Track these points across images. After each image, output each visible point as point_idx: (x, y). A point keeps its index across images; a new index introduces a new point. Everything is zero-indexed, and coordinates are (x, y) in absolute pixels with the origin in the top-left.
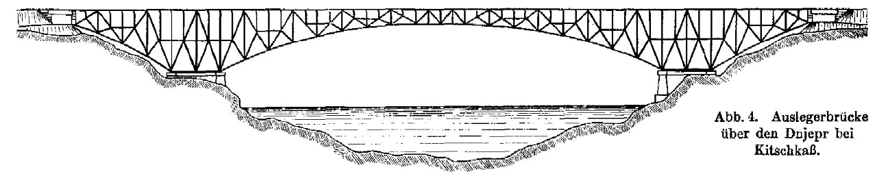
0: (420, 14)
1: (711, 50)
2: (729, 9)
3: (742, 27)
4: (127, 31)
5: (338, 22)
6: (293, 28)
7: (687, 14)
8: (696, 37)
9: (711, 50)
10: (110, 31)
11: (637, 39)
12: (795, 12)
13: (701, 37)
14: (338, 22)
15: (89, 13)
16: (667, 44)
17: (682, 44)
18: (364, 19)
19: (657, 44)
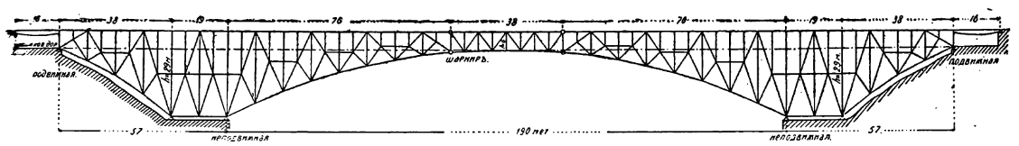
0: (530, 46)
1: (905, 63)
2: (917, 30)
3: (318, 54)
4: (121, 58)
5: (417, 46)
6: (815, 84)
7: (814, 35)
8: (454, 34)
9: (905, 63)
10: (935, 49)
11: (823, 91)
12: (936, 33)
13: (215, 72)
14: (417, 46)
15: (581, 35)
16: (736, 67)
17: (808, 80)
18: (396, 50)
19: (725, 67)
